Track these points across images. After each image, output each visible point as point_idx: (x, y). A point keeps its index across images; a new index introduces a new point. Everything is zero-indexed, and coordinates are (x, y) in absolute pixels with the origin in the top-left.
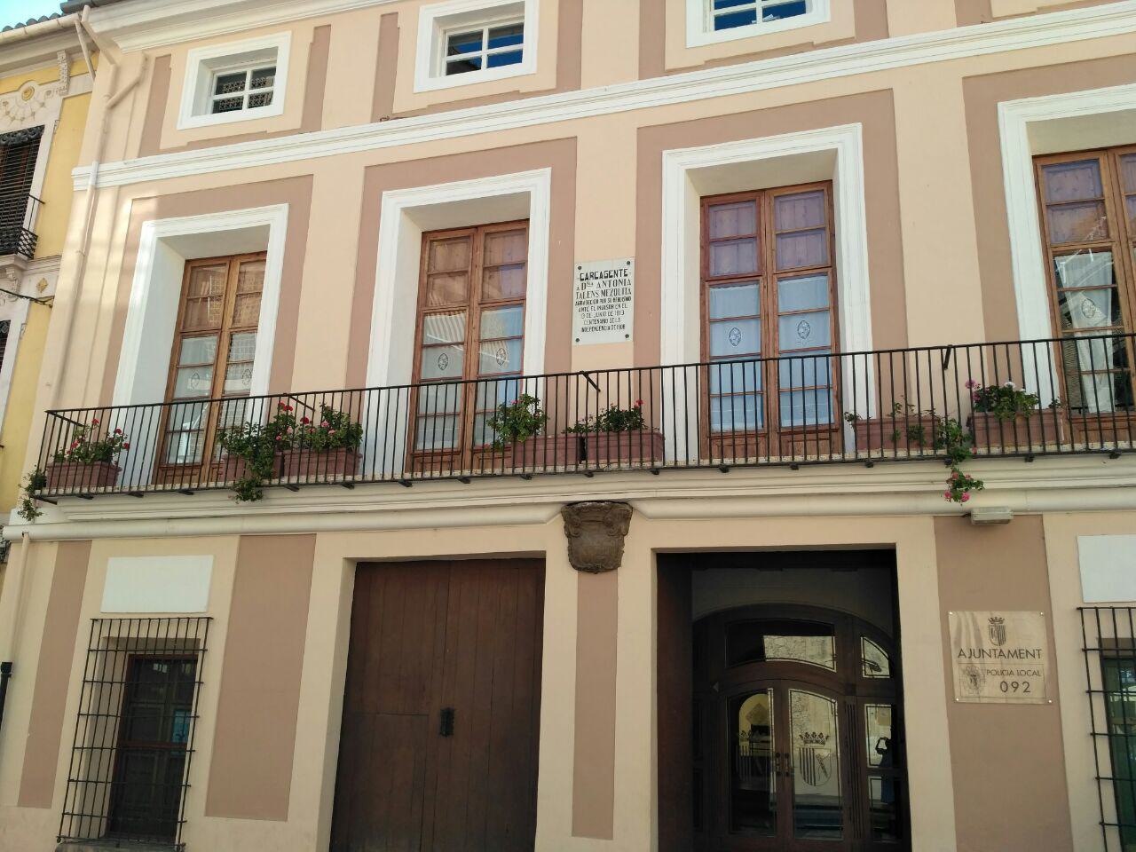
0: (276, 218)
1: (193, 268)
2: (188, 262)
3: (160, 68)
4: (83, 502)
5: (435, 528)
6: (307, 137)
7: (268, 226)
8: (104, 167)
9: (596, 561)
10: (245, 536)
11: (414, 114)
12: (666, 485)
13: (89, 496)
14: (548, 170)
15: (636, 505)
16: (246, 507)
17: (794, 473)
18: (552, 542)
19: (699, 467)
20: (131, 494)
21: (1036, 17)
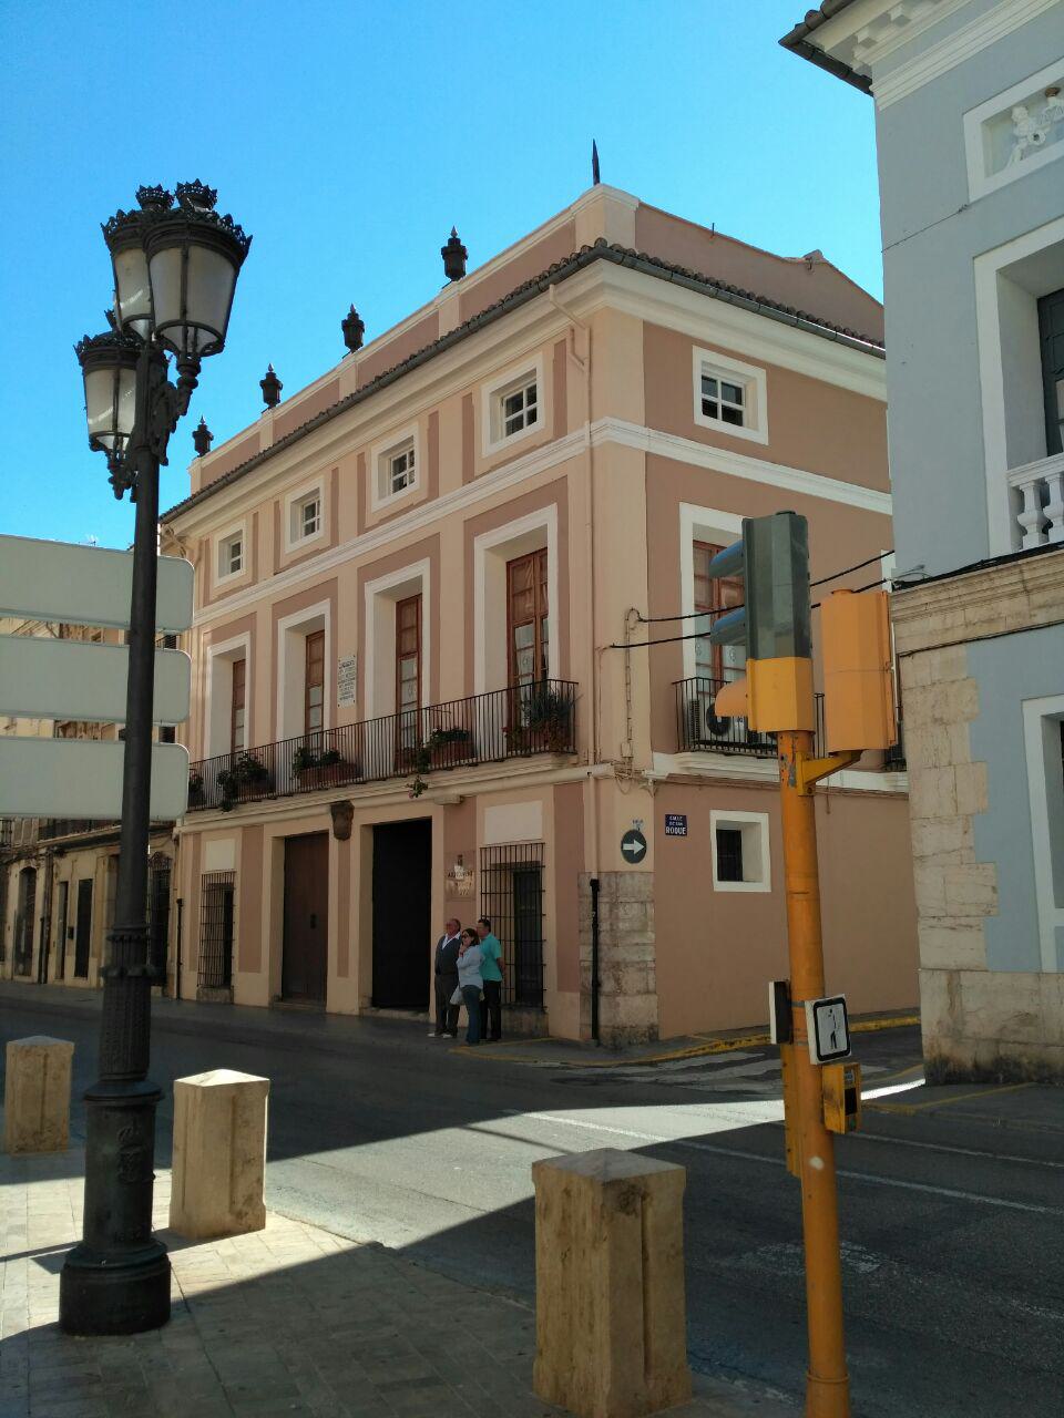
0: (547, 516)
1: (514, 568)
2: (508, 563)
3: (205, 545)
4: (499, 764)
5: (298, 818)
6: (433, 503)
7: (421, 576)
8: (595, 426)
9: (343, 835)
10: (244, 827)
11: (484, 474)
12: (366, 791)
13: (451, 769)
14: (248, 632)
15: (354, 804)
16: (227, 815)
17: (476, 769)
18: (326, 823)
19: (508, 758)
20: (496, 761)
21: (491, 474)
